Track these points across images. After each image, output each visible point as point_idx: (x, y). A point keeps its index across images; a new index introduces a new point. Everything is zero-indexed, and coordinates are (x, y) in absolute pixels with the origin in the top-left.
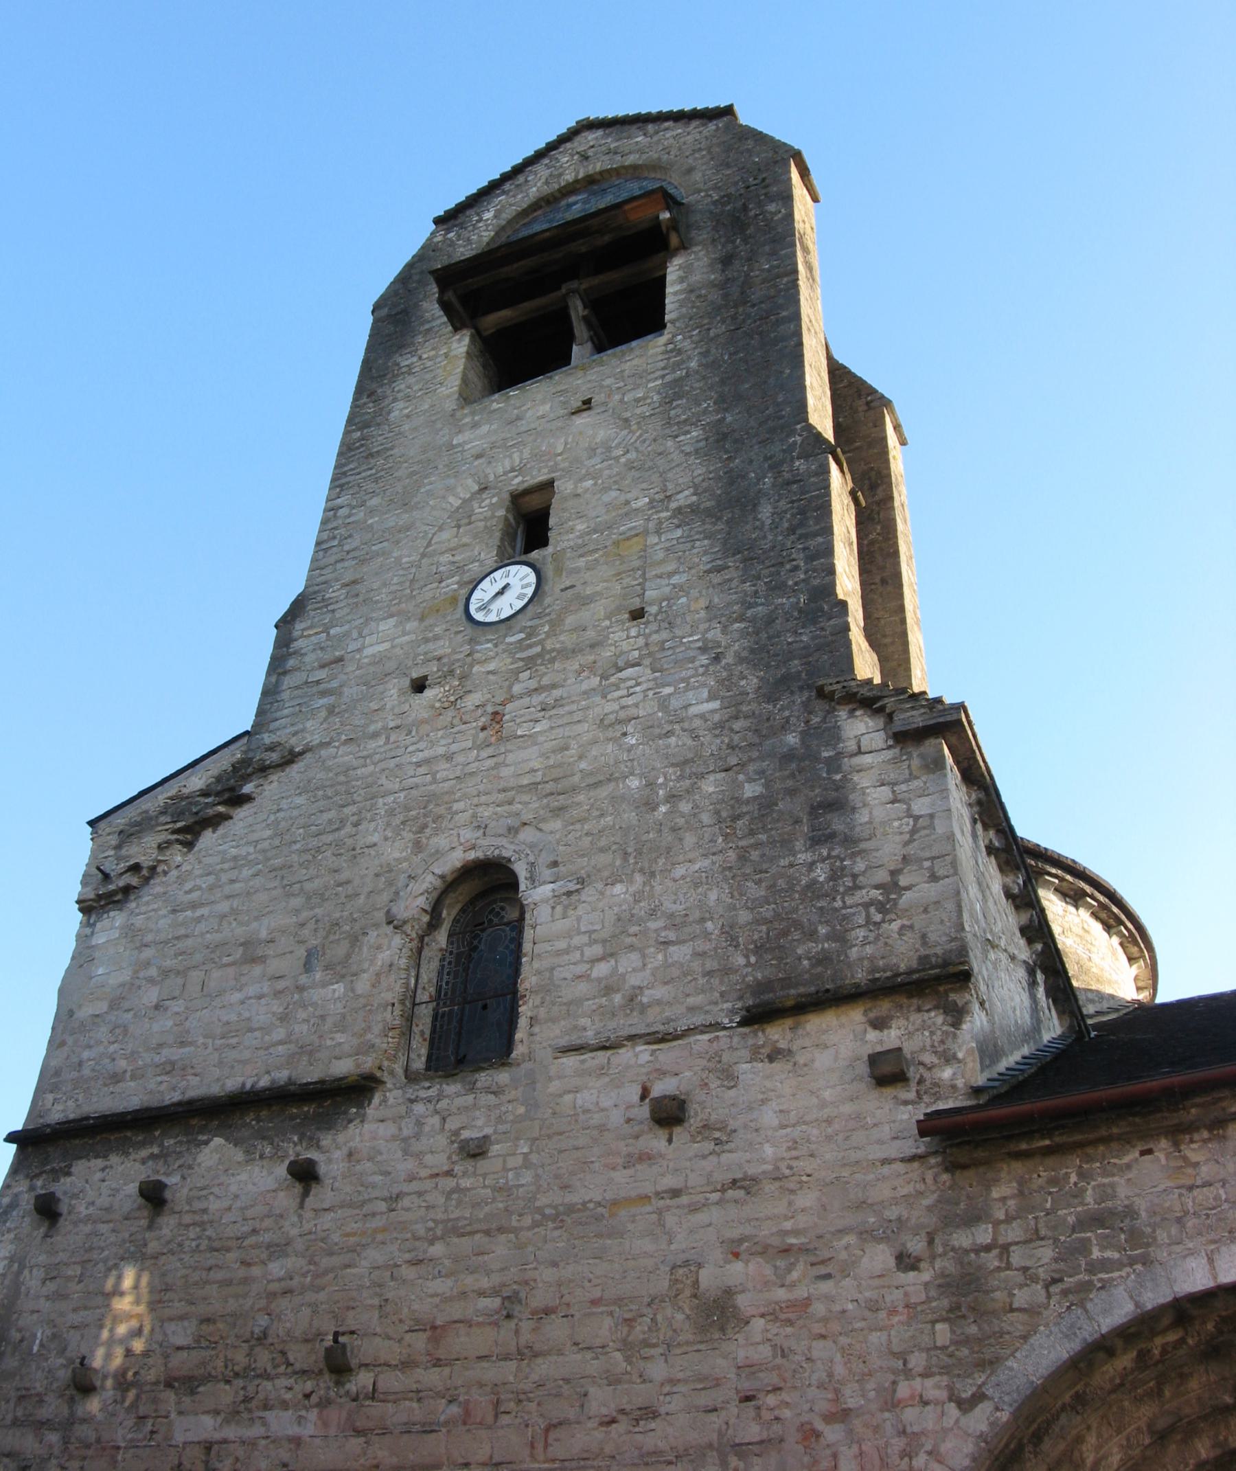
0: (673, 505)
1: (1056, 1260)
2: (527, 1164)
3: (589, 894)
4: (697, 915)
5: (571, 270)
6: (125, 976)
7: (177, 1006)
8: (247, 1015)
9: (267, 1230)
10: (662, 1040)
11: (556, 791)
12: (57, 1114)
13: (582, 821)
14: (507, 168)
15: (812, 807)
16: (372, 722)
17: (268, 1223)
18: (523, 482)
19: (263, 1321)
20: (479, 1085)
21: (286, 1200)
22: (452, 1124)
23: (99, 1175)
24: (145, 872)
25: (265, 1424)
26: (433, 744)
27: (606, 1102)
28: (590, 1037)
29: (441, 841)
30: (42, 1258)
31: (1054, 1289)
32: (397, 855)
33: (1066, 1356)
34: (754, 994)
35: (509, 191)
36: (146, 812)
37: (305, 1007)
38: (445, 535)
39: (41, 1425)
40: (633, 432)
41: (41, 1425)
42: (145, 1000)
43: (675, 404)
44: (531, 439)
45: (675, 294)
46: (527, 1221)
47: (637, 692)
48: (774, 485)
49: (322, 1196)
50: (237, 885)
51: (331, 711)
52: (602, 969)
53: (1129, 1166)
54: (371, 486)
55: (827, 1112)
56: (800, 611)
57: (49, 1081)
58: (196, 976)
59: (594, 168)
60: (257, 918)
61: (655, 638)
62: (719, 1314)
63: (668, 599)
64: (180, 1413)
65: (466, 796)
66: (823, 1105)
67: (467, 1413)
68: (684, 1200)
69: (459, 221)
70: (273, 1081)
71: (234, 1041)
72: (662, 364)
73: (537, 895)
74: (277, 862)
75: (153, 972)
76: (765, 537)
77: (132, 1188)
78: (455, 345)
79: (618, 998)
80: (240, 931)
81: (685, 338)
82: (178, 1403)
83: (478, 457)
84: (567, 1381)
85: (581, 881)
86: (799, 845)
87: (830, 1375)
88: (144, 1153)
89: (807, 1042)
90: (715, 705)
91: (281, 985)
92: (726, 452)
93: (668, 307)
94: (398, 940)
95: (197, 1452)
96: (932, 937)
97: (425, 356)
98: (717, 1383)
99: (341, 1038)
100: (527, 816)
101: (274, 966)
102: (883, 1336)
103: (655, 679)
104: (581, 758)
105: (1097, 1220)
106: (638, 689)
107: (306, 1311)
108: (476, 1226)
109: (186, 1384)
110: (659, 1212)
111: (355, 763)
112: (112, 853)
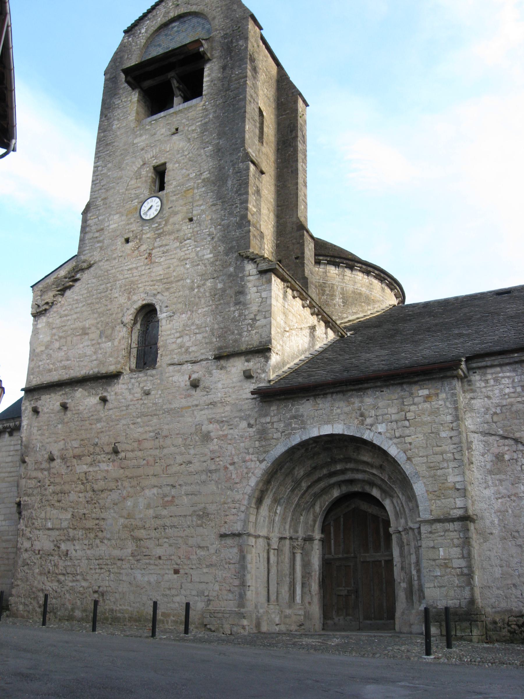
0: (203, 177)
1: (284, 427)
2: (161, 397)
3: (176, 317)
4: (204, 325)
5: (170, 67)
6: (49, 338)
7: (65, 348)
8: (85, 351)
9: (95, 415)
10: (194, 363)
11: (167, 282)
12: (36, 382)
13: (174, 293)
14: (149, 7)
15: (236, 293)
16: (114, 254)
17: (96, 413)
18: (157, 162)
19: (97, 440)
20: (148, 374)
21: (100, 407)
22: (141, 385)
23: (48, 400)
24: (50, 304)
25: (99, 467)
26: (132, 263)
27: (180, 380)
28: (176, 361)
29: (135, 298)
30: (36, 424)
31: (283, 434)
32: (123, 301)
33: (284, 451)
34: (218, 350)
35: (151, 18)
36: (48, 283)
37: (101, 349)
38: (133, 182)
39: (42, 470)
40: (191, 145)
41: (42, 470)
42: (55, 346)
43: (205, 133)
44: (159, 144)
45: (207, 82)
46: (161, 412)
47: (190, 250)
48: (233, 173)
49: (109, 405)
50: (78, 309)
51: (101, 248)
52: (179, 341)
53: (303, 403)
54: (108, 158)
55: (234, 385)
56: (237, 223)
57: (31, 372)
58: (69, 339)
59: (181, 11)
60: (85, 321)
61: (195, 229)
62: (206, 437)
63: (200, 215)
64: (78, 465)
65: (142, 283)
66: (233, 383)
67: (148, 463)
68: (199, 407)
69: (133, 32)
70: (94, 372)
71: (82, 359)
72: (201, 115)
73: (161, 316)
74: (89, 302)
75: (57, 337)
76: (228, 194)
77: (58, 404)
78: (133, 97)
79: (183, 349)
80: (80, 324)
81: (209, 103)
82: (77, 462)
83: (142, 149)
84: (171, 455)
85: (174, 313)
86: (231, 305)
87: (231, 453)
88: (61, 393)
89: (230, 365)
90: (211, 255)
91: (94, 342)
92: (220, 157)
93: (204, 88)
94: (125, 329)
95: (84, 475)
96: (263, 336)
97: (123, 100)
98: (206, 455)
99: (111, 359)
100: (159, 290)
101: (92, 336)
102: (244, 444)
103: (195, 245)
104: (174, 271)
105: (294, 417)
106: (190, 248)
107: (107, 437)
108: (148, 414)
109: (78, 457)
110: (193, 411)
111: (109, 268)
112: (39, 297)
